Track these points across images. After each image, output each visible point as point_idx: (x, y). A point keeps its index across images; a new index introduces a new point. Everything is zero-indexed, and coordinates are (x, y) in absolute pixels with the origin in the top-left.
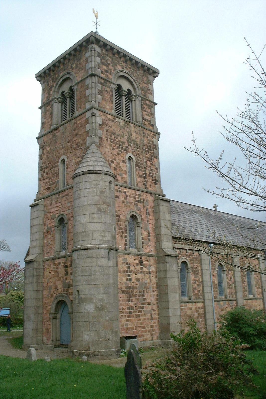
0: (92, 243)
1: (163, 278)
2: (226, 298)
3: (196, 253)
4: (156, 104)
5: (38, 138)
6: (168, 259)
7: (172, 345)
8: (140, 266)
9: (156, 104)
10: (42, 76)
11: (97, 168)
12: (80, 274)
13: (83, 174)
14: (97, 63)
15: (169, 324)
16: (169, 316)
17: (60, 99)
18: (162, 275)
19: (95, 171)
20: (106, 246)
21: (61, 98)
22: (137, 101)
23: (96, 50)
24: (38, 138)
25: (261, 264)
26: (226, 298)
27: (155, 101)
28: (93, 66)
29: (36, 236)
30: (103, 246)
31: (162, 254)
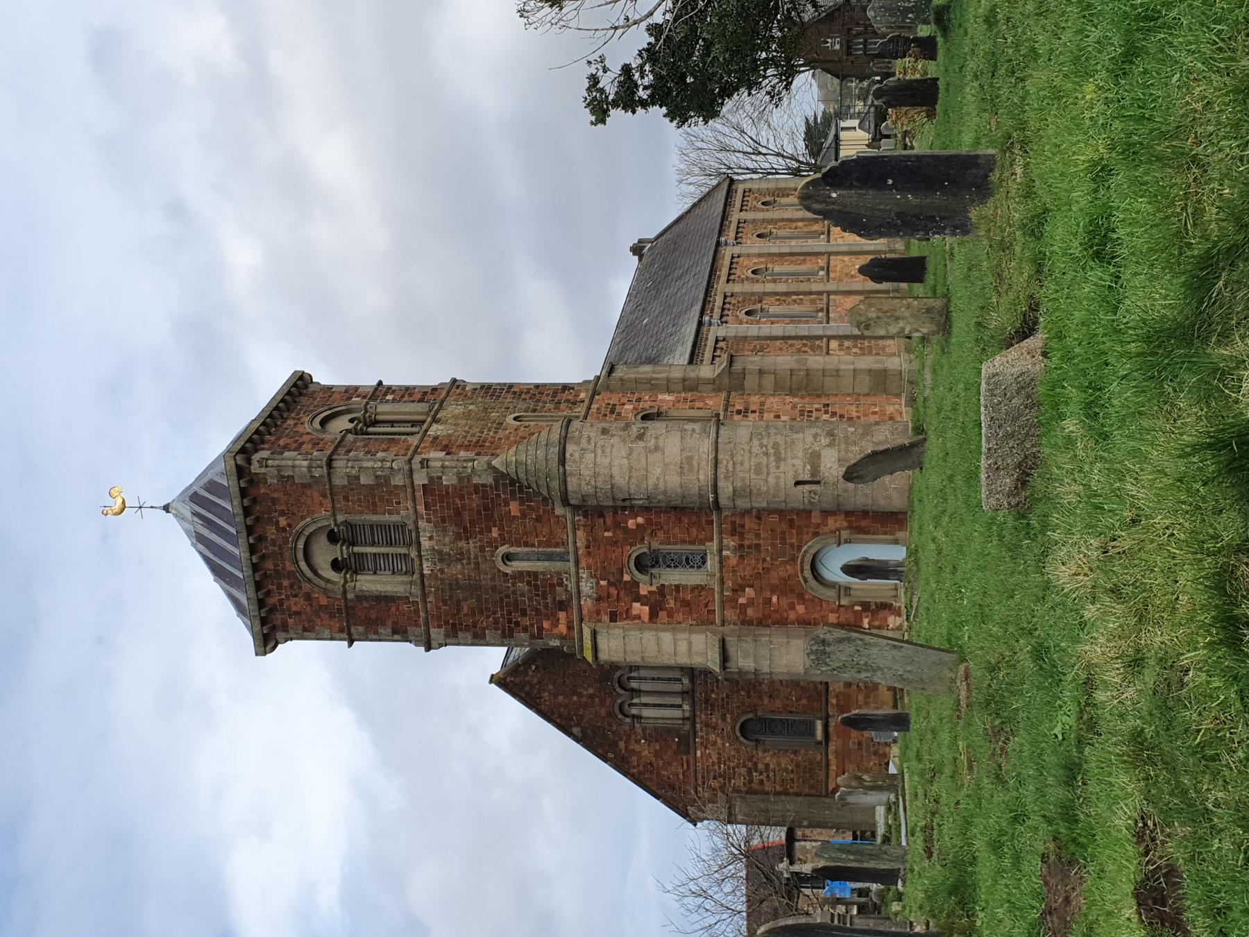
0: (706, 451)
1: (776, 382)
2: (822, 310)
3: (721, 344)
4: (380, 383)
5: (428, 648)
6: (737, 366)
7: (1006, 643)
8: (750, 414)
9: (380, 383)
10: (266, 641)
11: (555, 436)
12: (764, 477)
13: (564, 466)
14: (299, 457)
15: (870, 371)
16: (854, 370)
17: (348, 576)
18: (769, 381)
19: (562, 441)
20: (713, 429)
21: (346, 573)
22: (378, 410)
23: (265, 456)
24: (428, 648)
25: (732, 667)
26: (822, 310)
27: (375, 383)
28: (305, 463)
29: (721, 262)
30: (713, 434)
31: (726, 380)
